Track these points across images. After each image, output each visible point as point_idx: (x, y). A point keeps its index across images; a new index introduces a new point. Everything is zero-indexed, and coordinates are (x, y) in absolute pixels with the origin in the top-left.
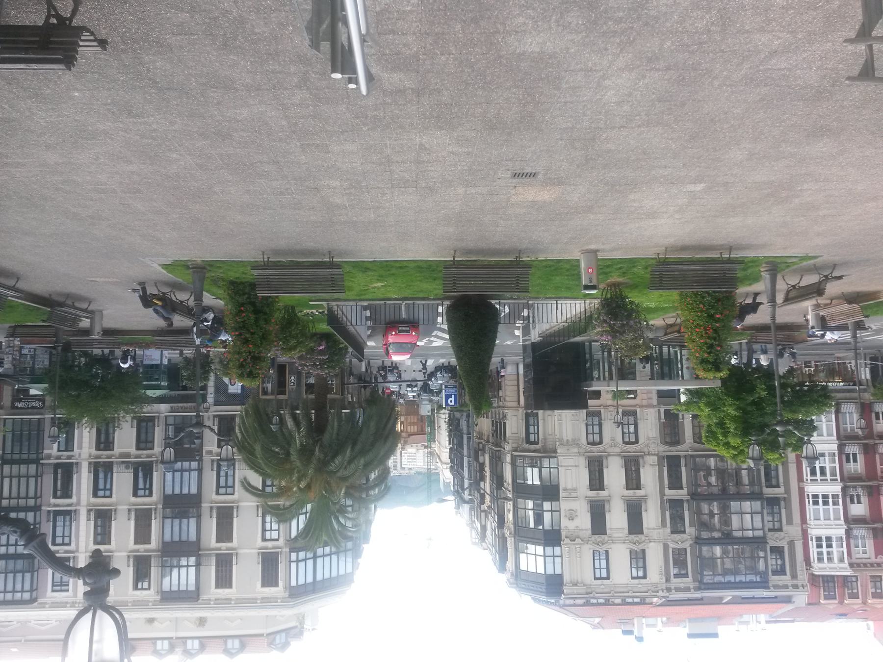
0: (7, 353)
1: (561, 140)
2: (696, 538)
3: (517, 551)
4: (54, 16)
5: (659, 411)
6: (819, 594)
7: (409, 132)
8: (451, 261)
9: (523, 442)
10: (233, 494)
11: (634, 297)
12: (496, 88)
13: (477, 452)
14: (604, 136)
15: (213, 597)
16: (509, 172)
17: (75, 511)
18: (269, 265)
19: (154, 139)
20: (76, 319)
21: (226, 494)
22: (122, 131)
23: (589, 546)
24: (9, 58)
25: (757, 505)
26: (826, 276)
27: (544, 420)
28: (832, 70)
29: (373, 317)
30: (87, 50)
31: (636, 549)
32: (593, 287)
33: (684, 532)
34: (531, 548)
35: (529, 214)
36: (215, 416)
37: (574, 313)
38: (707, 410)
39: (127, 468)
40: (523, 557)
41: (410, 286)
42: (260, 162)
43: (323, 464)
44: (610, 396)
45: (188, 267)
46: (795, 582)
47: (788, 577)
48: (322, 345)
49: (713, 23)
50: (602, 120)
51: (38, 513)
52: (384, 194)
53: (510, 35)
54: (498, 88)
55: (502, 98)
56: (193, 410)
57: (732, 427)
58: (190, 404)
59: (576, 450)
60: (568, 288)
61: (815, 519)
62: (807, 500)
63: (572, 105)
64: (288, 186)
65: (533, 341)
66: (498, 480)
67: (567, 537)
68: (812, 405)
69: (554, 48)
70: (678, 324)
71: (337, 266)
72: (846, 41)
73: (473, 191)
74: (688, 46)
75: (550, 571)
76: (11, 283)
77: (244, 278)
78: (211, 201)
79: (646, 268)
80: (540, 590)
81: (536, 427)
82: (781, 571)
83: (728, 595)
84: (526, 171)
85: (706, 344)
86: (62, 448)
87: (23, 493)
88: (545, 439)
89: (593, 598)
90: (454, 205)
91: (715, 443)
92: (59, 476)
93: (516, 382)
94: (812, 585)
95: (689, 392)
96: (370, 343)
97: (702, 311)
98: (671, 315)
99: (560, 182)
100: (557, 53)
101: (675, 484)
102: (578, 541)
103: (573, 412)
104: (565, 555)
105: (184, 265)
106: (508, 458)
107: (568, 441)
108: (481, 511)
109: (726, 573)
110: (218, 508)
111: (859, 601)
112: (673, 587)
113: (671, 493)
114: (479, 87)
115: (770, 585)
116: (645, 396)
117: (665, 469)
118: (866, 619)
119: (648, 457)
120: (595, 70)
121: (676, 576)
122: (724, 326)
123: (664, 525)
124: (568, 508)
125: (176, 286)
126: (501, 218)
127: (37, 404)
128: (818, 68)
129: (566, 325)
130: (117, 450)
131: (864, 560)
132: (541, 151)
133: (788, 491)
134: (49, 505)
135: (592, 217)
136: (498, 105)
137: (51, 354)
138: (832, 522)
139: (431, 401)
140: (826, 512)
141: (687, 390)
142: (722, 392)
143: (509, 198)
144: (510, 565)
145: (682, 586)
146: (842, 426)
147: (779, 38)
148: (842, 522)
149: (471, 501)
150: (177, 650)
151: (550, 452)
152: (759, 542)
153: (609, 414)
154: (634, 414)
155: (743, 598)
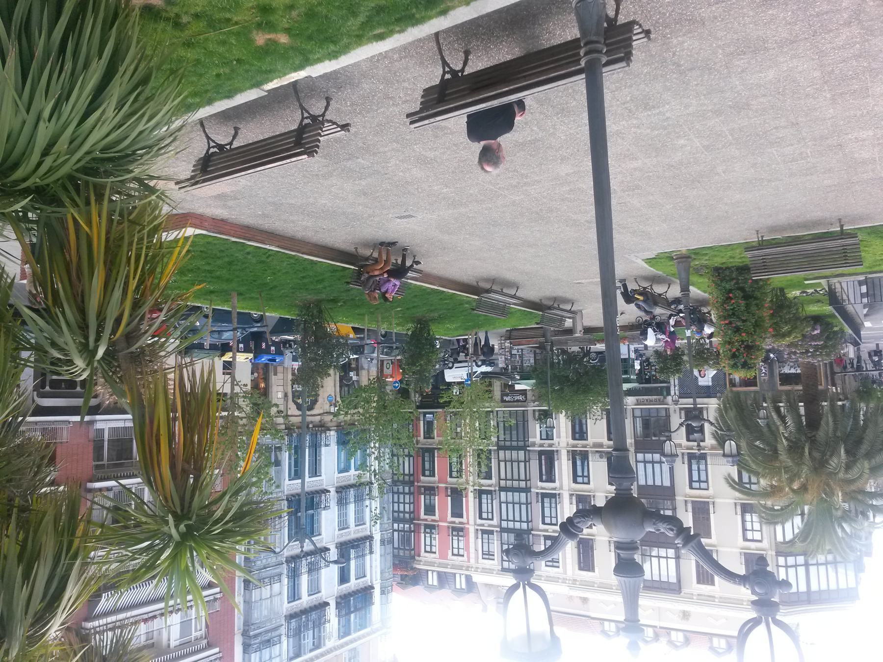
0: (501, 354)
4: (448, 72)
10: (707, 489)
15: (695, 592)
17: (559, 494)
18: (764, 244)
19: (665, 128)
20: (562, 320)
21: (700, 489)
22: (635, 127)
24: (452, 108)
29: (871, 292)
30: (638, 43)
36: (681, 409)
39: (601, 457)
42: (776, 128)
43: (819, 466)
45: (672, 258)
48: (816, 329)
51: (529, 494)
56: (658, 402)
58: (655, 397)
64: (803, 150)
71: (852, 235)
76: (512, 292)
77: (731, 262)
78: (711, 183)
86: (544, 437)
87: (516, 477)
92: (543, 462)
96: (867, 324)
105: (668, 257)
110: (693, 502)
125: (655, 280)
127: (521, 398)
130: (591, 440)
134: (537, 488)
137: (535, 353)
150: (661, 639)
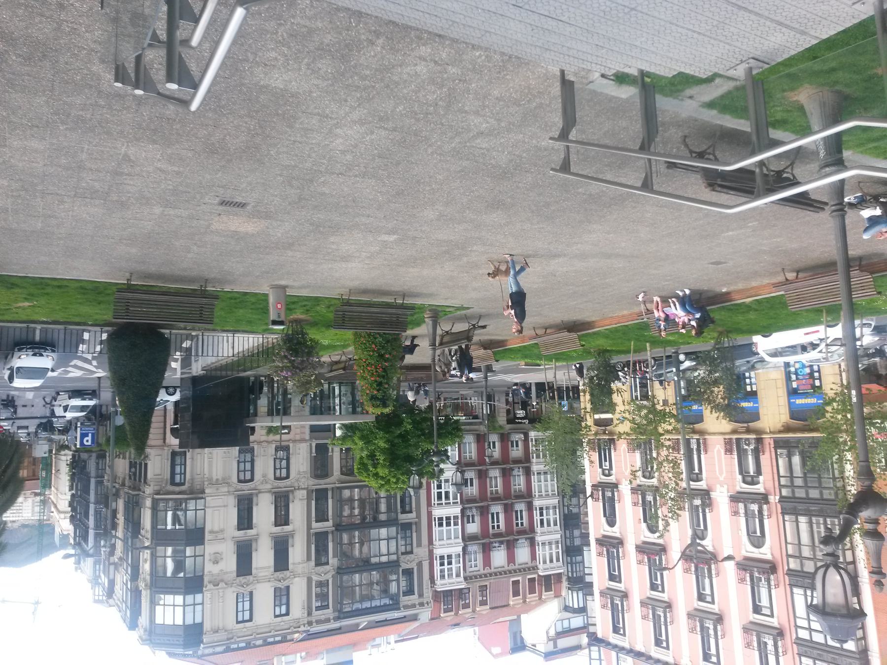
1: (281, 176)
2: (338, 568)
3: (153, 603)
5: (311, 445)
6: (440, 608)
7: (115, 139)
8: (124, 284)
9: (166, 484)
11: (313, 334)
12: (228, 114)
13: (104, 500)
14: (323, 179)
16: (218, 199)
23: (233, 589)
25: (393, 530)
26: (474, 325)
27: (192, 458)
28: (518, 156)
31: (280, 586)
32: (281, 323)
33: (327, 563)
34: (169, 599)
35: (227, 243)
37: (246, 347)
38: (361, 443)
40: (159, 609)
41: (66, 308)
44: (264, 432)
46: (421, 600)
47: (416, 596)
49: (441, 99)
50: (324, 164)
52: (62, 202)
53: (259, 66)
54: (231, 114)
55: (232, 125)
57: (381, 458)
59: (226, 489)
60: (250, 322)
61: (439, 540)
62: (434, 523)
63: (300, 145)
65: (195, 374)
66: (134, 525)
67: (210, 582)
68: (447, 437)
69: (298, 88)
70: (343, 362)
72: (551, 138)
73: (172, 212)
74: (416, 114)
75: (189, 621)
79: (329, 307)
80: (178, 643)
81: (183, 466)
82: (410, 592)
83: (364, 621)
84: (235, 200)
85: (376, 381)
88: (192, 479)
89: (233, 643)
90: (146, 223)
91: (365, 475)
93: (162, 418)
94: (435, 601)
95: (345, 427)
97: (373, 351)
98: (336, 353)
99: (267, 216)
100: (300, 93)
101: (321, 517)
102: (222, 585)
103: (225, 449)
104: (207, 601)
106: (148, 503)
107: (217, 480)
108: (110, 564)
109: (363, 599)
111: (470, 610)
112: (314, 621)
113: (317, 526)
114: (210, 109)
115: (401, 606)
116: (298, 431)
117: (313, 502)
118: (474, 625)
119: (298, 491)
120: (331, 118)
121: (318, 608)
122: (391, 366)
123: (309, 558)
124: (213, 551)
126: (195, 244)
128: (509, 153)
129: (235, 359)
131: (475, 573)
132: (257, 183)
133: (419, 516)
135: (290, 253)
136: (226, 131)
138: (452, 541)
139: (50, 440)
140: (449, 532)
141: (343, 425)
142: (374, 426)
143: (210, 225)
144: (144, 620)
145: (323, 617)
146: (463, 455)
147: (488, 122)
148: (460, 540)
149: (97, 553)
151: (197, 493)
152: (393, 565)
153: (262, 450)
154: (287, 449)
155: (377, 622)
